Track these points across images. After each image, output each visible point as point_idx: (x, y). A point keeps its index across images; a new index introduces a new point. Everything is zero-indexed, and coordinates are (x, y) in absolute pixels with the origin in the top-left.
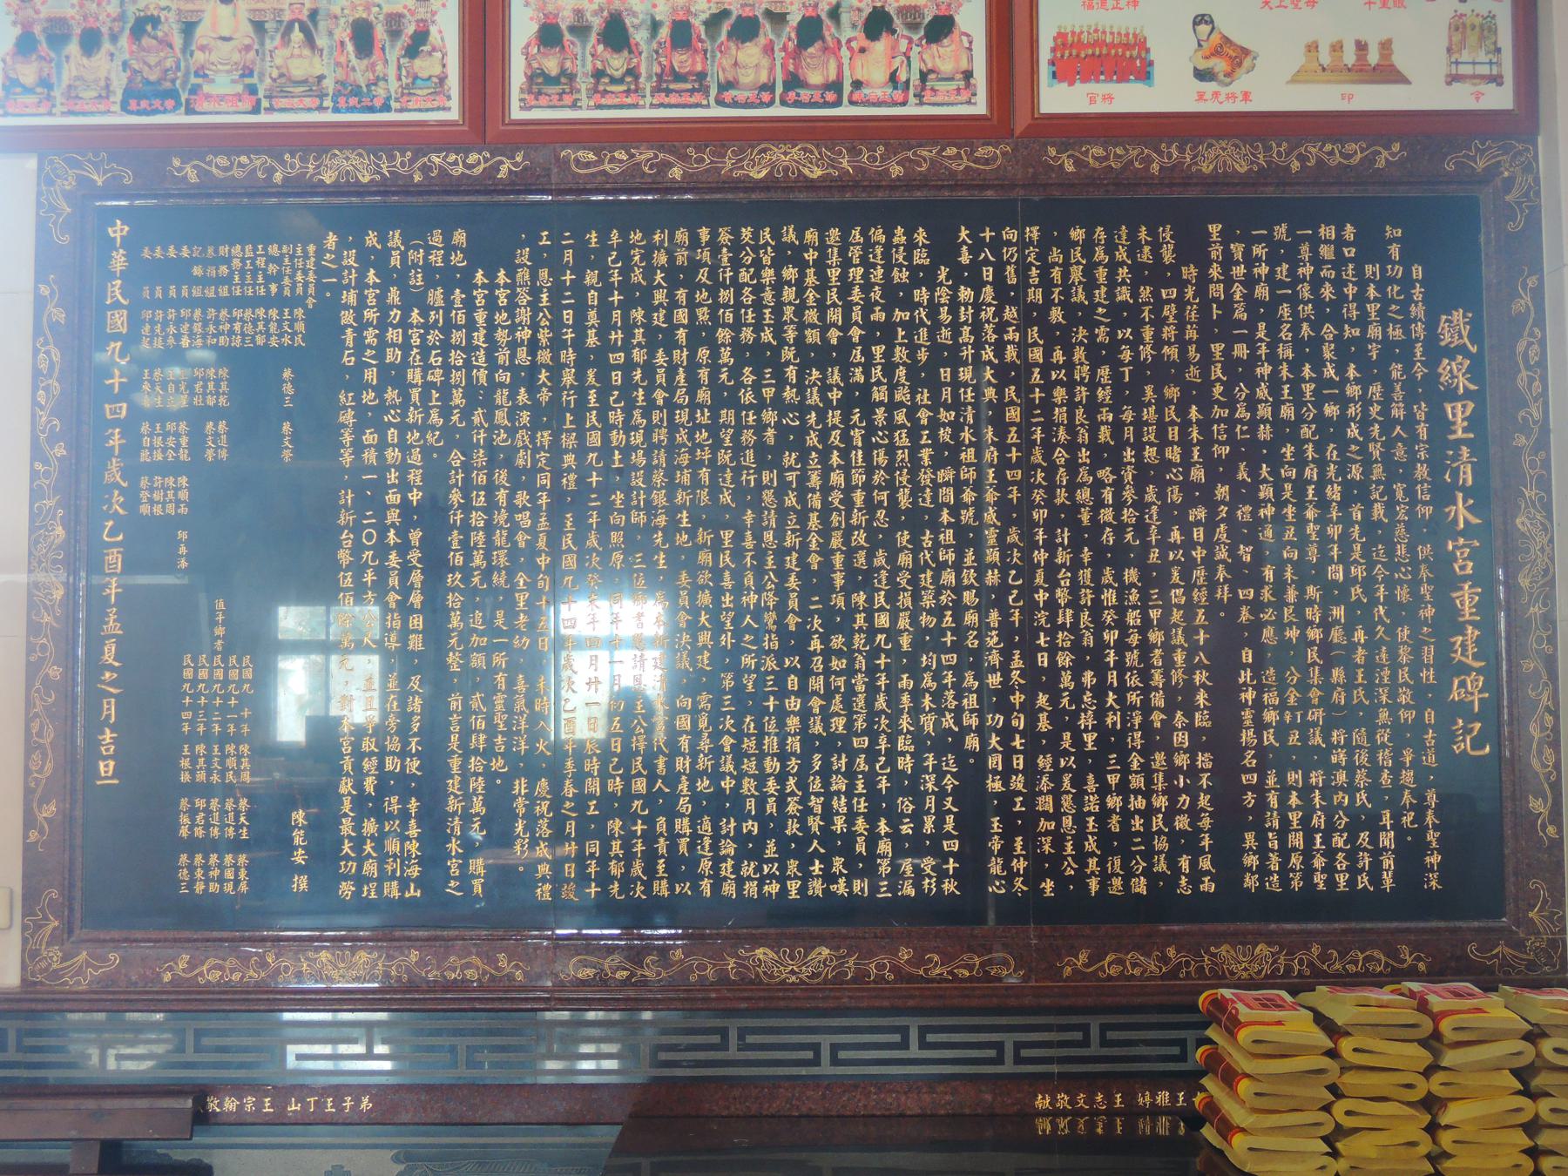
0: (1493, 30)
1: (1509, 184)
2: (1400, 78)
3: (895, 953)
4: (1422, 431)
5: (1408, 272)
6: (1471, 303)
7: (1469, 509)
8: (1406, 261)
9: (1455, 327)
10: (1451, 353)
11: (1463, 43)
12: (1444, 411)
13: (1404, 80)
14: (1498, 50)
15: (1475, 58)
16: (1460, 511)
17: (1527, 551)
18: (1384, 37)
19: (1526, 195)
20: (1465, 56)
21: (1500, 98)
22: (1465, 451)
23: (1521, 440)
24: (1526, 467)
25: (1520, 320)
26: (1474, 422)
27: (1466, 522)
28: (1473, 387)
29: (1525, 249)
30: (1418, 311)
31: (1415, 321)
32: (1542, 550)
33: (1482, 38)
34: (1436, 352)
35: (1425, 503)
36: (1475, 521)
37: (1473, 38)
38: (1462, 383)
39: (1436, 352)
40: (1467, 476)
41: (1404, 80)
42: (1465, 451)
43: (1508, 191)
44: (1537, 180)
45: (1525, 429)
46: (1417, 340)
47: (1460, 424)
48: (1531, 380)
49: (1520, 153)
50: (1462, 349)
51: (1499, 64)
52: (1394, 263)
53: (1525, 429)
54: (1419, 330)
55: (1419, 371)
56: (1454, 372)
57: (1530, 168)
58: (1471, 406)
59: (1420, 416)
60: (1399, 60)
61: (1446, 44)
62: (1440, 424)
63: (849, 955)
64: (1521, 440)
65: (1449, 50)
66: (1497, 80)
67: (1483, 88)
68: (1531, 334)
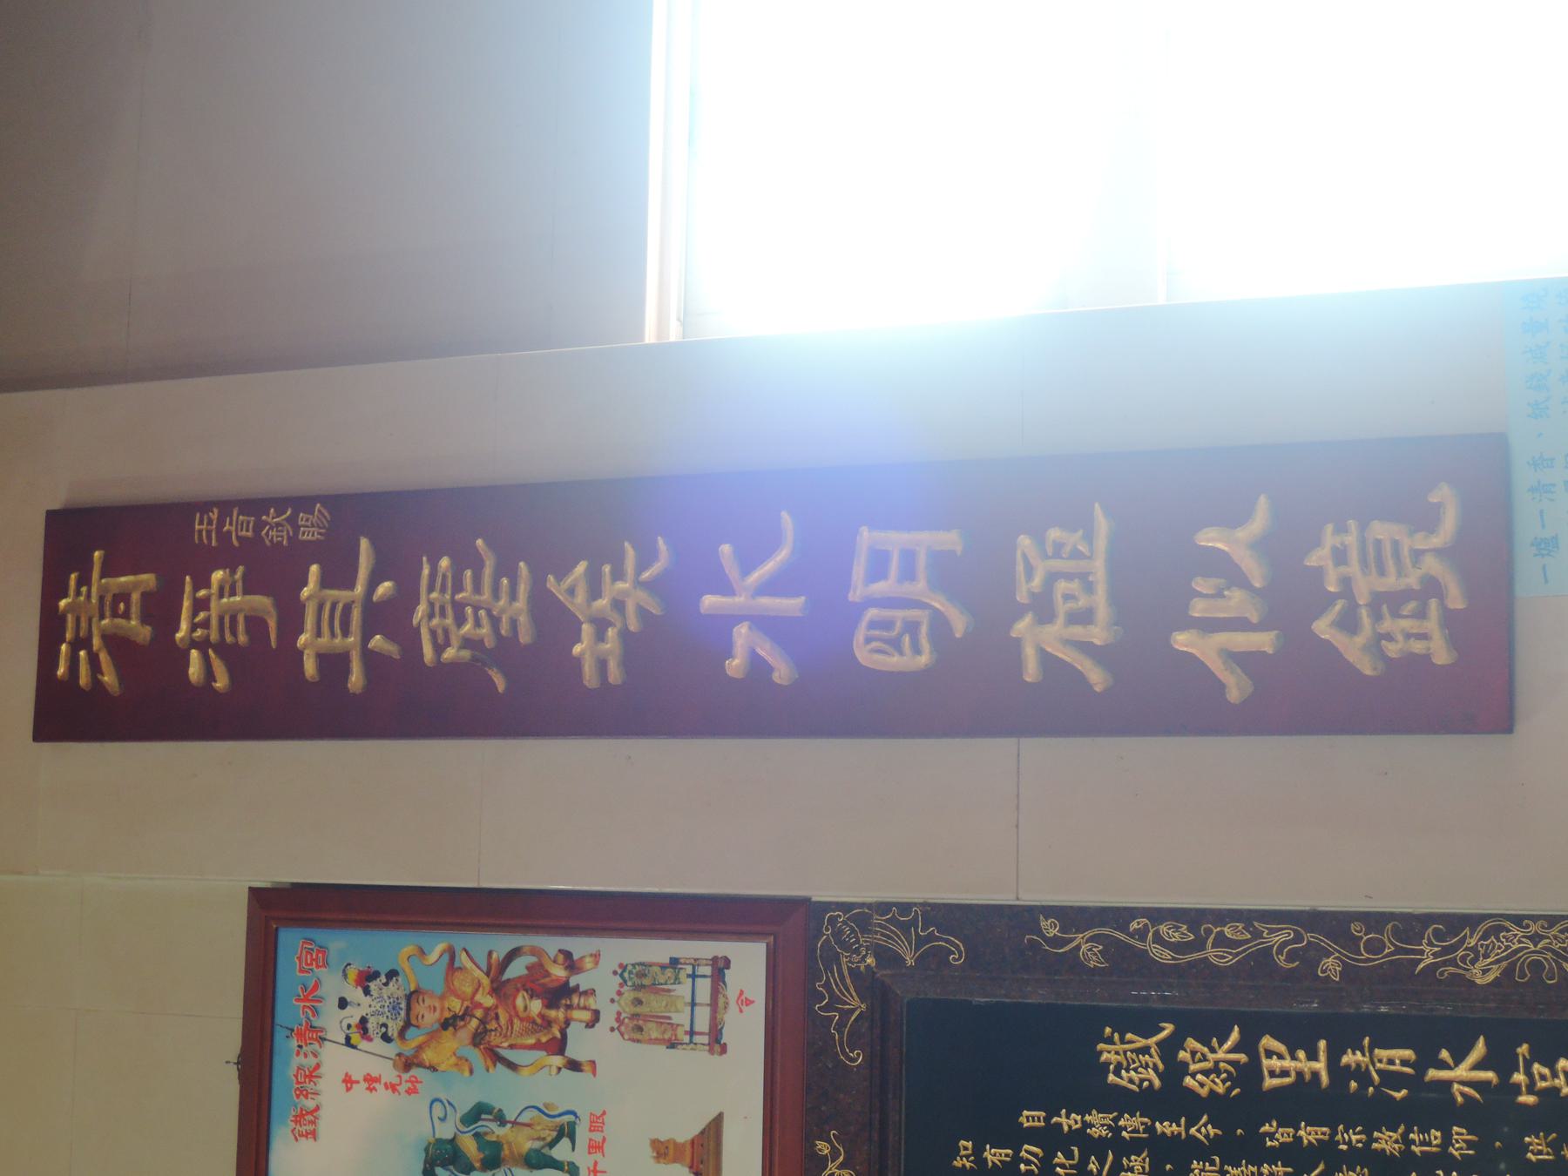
0: (643, 969)
1: (887, 958)
2: (714, 1129)
3: (1347, 971)
4: (1310, 1134)
5: (1032, 1136)
6: (1088, 1026)
7: (1459, 1059)
8: (1015, 1137)
9: (1130, 1061)
10: (1174, 1071)
11: (663, 1021)
12: (1276, 1090)
13: (716, 1125)
14: (674, 962)
15: (684, 1002)
16: (1463, 1073)
17: (1537, 966)
18: (648, 1152)
19: (905, 928)
20: (681, 1018)
21: (749, 963)
22: (1349, 1058)
23: (1331, 966)
24: (1378, 959)
25: (1114, 951)
26: (1299, 1037)
27: (1477, 1066)
28: (1235, 1035)
29: (997, 931)
30: (1099, 1123)
31: (1116, 1130)
32: (1535, 938)
33: (654, 988)
34: (1170, 1098)
35: (1447, 1140)
36: (1479, 1049)
37: (654, 1004)
38: (1224, 1053)
39: (1170, 1098)
40: (1398, 1057)
41: (716, 1125)
42: (1349, 1058)
43: (898, 960)
44: (883, 908)
45: (1309, 958)
46: (1150, 1129)
47: (1301, 1063)
48: (1221, 941)
49: (838, 934)
50: (1169, 1049)
51: (696, 963)
52: (1017, 1159)
53: (1309, 958)
54: (1132, 1123)
55: (1204, 1130)
56: (1208, 1066)
57: (862, 916)
58: (1268, 1042)
59: (1284, 1135)
60: (685, 1130)
61: (662, 1049)
62: (1300, 1101)
63: (1432, 968)
64: (1331, 966)
65: (672, 1045)
66: (720, 967)
67: (731, 992)
68: (1142, 934)
